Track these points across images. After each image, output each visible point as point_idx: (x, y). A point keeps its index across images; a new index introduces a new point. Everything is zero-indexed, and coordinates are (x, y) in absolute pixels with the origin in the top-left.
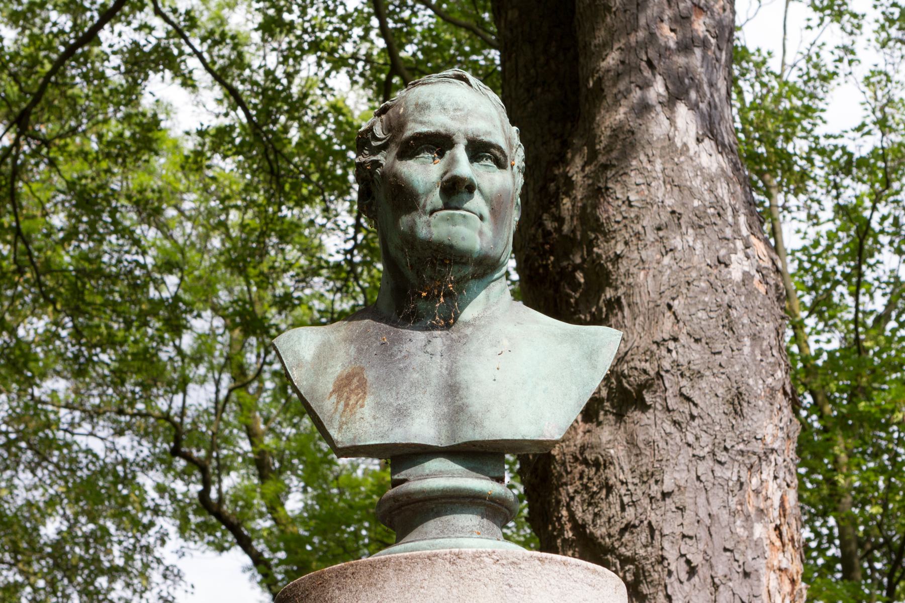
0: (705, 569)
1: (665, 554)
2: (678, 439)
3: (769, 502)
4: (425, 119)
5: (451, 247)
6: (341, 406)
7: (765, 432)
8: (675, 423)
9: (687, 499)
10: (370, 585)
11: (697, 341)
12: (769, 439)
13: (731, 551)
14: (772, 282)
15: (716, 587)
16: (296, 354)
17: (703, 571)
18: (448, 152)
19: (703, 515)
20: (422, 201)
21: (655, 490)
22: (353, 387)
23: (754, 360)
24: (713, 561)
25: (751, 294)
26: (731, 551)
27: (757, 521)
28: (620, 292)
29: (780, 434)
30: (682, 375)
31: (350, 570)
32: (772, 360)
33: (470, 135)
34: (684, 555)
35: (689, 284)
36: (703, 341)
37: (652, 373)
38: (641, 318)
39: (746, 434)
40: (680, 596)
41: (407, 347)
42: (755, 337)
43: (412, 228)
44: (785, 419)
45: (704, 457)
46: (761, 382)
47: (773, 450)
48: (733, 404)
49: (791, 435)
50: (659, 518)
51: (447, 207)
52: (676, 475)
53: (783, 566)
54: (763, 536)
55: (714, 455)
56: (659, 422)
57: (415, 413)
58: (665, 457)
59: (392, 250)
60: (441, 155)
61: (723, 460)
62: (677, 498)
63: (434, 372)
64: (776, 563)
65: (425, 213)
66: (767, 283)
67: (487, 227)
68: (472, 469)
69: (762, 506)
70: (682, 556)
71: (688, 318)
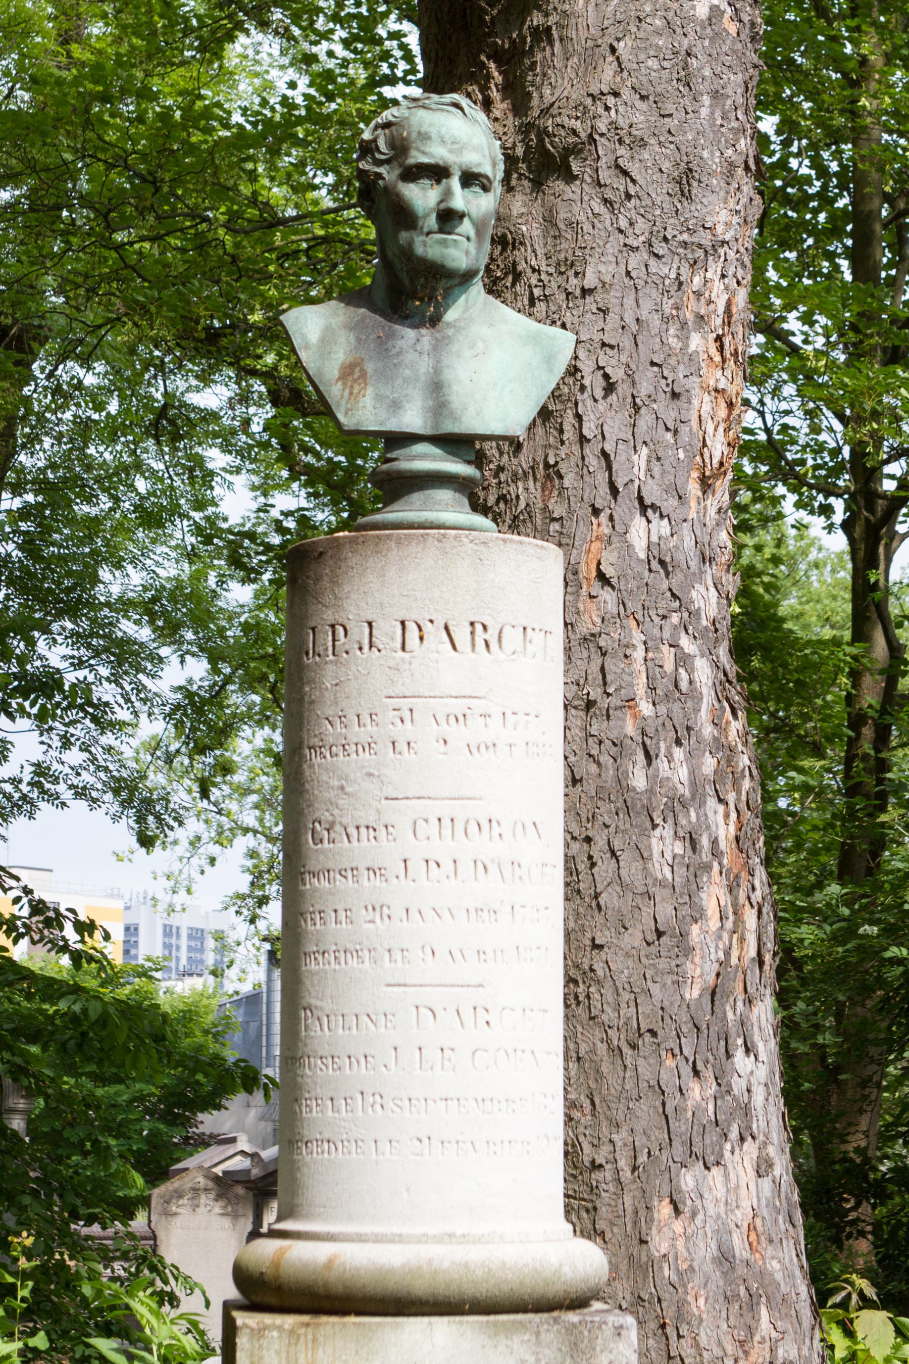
0: (625, 386)
1: (579, 364)
2: (608, 223)
3: (712, 306)
4: (427, 150)
5: (443, 266)
6: (346, 393)
7: (716, 219)
8: (606, 201)
9: (611, 299)
10: (377, 552)
11: (643, 98)
12: (720, 229)
13: (660, 366)
14: (746, 18)
15: (637, 408)
16: (304, 336)
17: (623, 389)
18: (444, 181)
19: (629, 319)
20: (420, 224)
21: (574, 284)
22: (356, 376)
23: (713, 125)
24: (636, 377)
25: (718, 37)
26: (660, 366)
27: (695, 330)
28: (553, 19)
29: (736, 220)
30: (620, 141)
31: (361, 540)
32: (735, 124)
33: (464, 167)
34: (603, 368)
35: (640, 20)
36: (651, 98)
37: (583, 135)
38: (576, 60)
39: (694, 221)
40: (592, 417)
41: (400, 343)
42: (716, 95)
43: (411, 244)
44: (744, 200)
45: (637, 248)
46: (718, 154)
47: (724, 243)
48: (680, 183)
49: (749, 219)
50: (576, 320)
51: (441, 231)
52: (602, 268)
53: (721, 386)
54: (700, 349)
55: (650, 245)
56: (586, 198)
57: (407, 406)
58: (590, 244)
59: (389, 254)
60: (438, 182)
61: (661, 253)
62: (599, 296)
63: (423, 370)
64: (712, 383)
65: (422, 233)
66: (740, 21)
67: (472, 247)
68: (450, 453)
69: (703, 312)
70: (600, 368)
71: (635, 66)
